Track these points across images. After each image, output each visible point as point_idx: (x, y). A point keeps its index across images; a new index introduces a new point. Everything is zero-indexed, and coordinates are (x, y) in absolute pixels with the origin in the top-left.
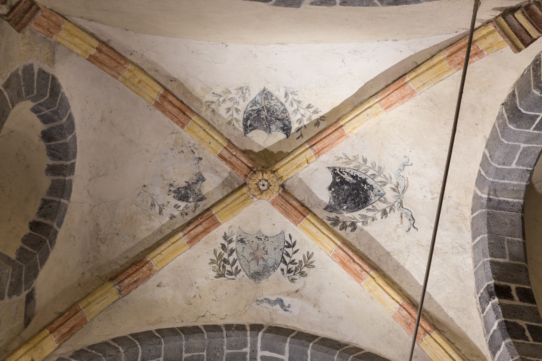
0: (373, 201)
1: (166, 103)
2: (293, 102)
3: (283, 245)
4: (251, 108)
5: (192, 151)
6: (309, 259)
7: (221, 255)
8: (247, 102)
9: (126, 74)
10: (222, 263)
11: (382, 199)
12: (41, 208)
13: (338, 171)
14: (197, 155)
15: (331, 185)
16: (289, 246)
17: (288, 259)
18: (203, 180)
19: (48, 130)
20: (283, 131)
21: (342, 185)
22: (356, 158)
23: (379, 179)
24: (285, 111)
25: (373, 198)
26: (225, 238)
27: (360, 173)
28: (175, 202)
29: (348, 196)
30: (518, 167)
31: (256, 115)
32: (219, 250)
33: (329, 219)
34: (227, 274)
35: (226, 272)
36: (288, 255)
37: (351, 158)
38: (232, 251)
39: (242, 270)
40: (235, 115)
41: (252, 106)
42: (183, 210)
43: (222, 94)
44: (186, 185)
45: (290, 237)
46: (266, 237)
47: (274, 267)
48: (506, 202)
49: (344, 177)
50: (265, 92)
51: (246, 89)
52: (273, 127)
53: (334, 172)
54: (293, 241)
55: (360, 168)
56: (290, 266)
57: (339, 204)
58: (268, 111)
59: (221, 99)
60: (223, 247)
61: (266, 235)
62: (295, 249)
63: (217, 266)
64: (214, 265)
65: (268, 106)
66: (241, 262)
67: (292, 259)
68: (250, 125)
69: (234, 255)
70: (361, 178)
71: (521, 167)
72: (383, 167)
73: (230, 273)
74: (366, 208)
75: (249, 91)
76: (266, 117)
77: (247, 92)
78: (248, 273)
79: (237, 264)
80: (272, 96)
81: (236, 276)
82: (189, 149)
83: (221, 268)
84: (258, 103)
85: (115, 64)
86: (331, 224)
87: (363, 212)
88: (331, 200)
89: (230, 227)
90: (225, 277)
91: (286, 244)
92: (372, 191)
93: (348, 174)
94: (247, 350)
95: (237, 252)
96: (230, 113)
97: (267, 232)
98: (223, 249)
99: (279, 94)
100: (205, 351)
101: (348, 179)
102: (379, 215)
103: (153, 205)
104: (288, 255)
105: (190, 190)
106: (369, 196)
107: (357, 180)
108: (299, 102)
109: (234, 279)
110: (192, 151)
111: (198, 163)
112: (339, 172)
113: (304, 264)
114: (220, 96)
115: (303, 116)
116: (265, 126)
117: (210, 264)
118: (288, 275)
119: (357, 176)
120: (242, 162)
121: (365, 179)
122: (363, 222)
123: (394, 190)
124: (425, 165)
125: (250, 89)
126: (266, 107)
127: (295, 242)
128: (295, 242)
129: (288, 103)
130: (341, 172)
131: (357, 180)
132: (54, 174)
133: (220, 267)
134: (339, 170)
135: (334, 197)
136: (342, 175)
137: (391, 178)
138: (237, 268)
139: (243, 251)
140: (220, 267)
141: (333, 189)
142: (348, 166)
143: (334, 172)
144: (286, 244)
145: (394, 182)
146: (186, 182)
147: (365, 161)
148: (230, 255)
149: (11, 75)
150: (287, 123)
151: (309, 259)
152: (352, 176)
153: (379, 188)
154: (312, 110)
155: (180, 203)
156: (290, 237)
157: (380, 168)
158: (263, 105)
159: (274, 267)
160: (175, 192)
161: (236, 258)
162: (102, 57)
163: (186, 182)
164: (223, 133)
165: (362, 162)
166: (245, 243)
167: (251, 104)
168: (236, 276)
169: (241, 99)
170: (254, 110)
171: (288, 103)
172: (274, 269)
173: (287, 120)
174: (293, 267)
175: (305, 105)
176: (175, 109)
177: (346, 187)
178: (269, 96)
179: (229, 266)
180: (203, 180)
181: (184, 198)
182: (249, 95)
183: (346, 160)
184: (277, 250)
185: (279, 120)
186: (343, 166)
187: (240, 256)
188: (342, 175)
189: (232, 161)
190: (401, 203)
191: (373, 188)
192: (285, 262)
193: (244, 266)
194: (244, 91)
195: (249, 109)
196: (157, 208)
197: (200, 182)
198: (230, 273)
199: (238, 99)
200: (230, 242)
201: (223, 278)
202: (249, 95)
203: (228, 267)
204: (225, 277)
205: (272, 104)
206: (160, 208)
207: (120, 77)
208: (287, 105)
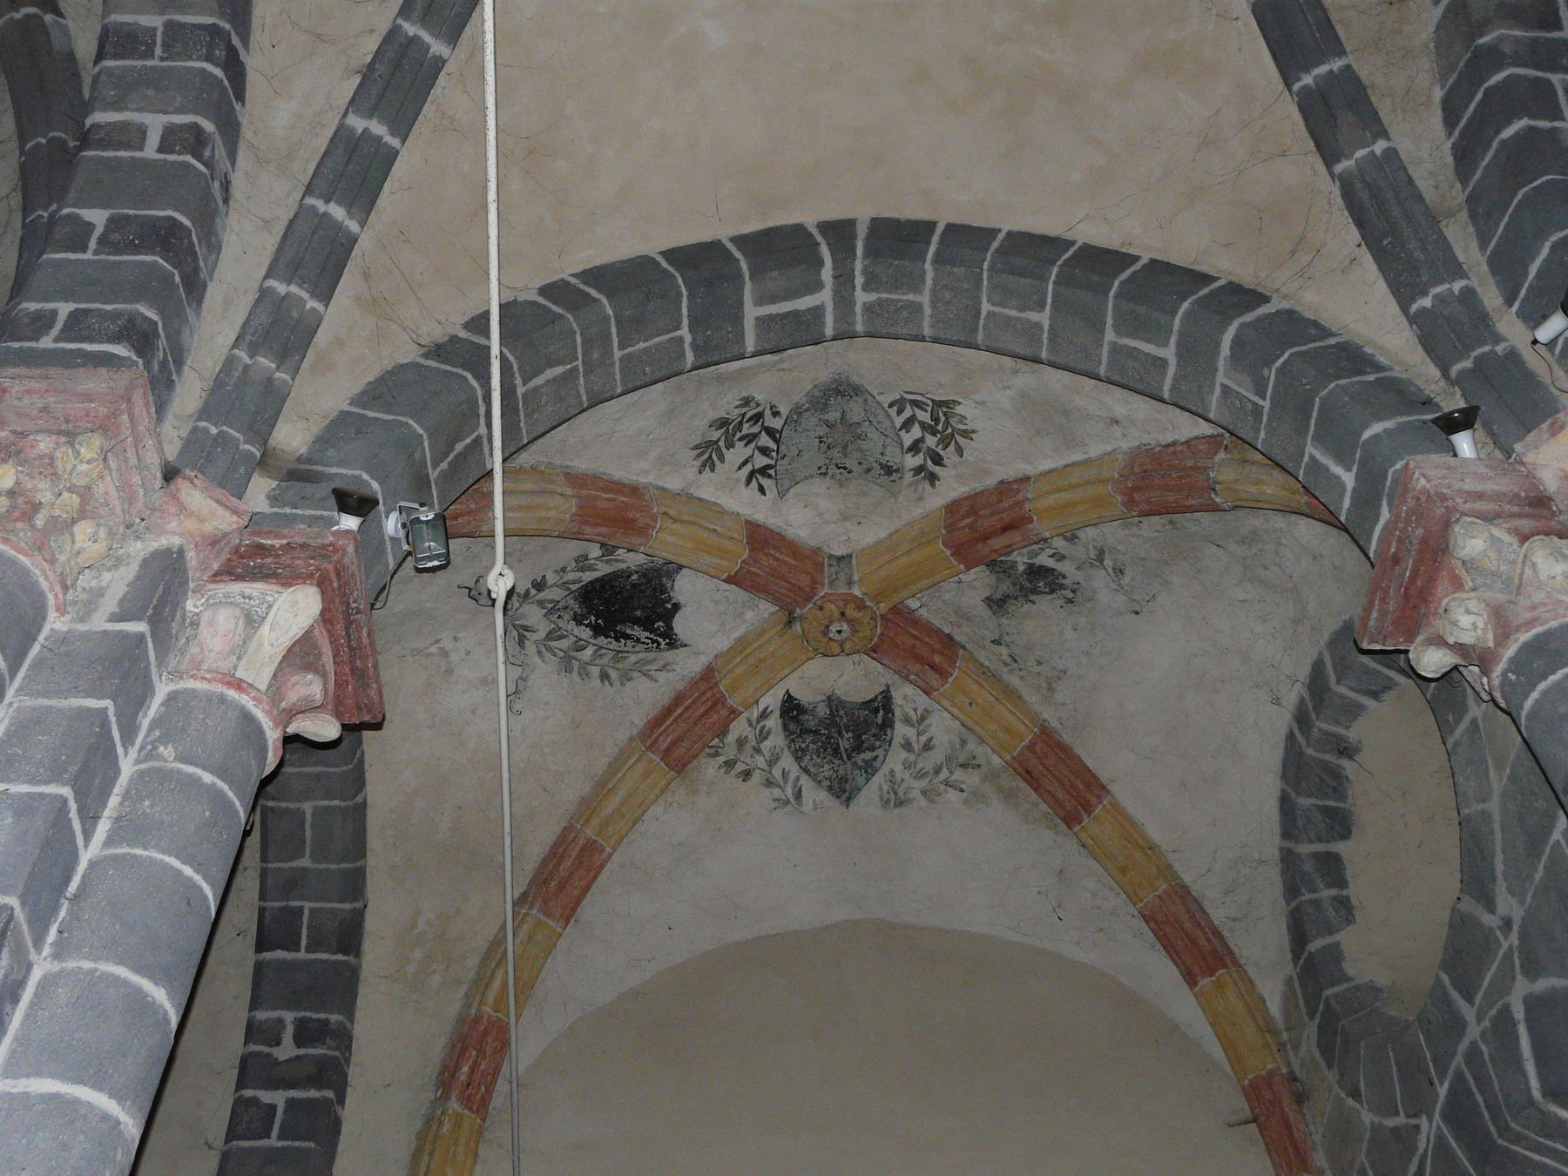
8: (885, 770)
14: (1003, 650)
16: (763, 471)
17: (765, 440)
18: (989, 601)
19: (1334, 839)
22: (626, 678)
23: (564, 644)
26: (933, 478)
28: (1064, 567)
30: (298, 805)
32: (949, 455)
36: (764, 451)
37: (635, 674)
38: (915, 448)
40: (910, 732)
41: (875, 759)
43: (942, 787)
45: (762, 490)
51: (888, 801)
52: (823, 711)
54: (754, 484)
58: (836, 751)
59: (944, 774)
60: (938, 460)
66: (887, 423)
67: (752, 445)
68: (876, 711)
69: (908, 439)
71: (290, 805)
73: (915, 403)
76: (840, 733)
77: (885, 796)
79: (899, 421)
80: (830, 789)
84: (860, 768)
87: (588, 577)
89: (920, 499)
91: (772, 472)
94: (862, 297)
96: (923, 739)
97: (819, 486)
99: (814, 794)
100: (984, 314)
101: (637, 632)
102: (551, 578)
104: (764, 451)
107: (616, 632)
108: (769, 783)
113: (721, 443)
114: (946, 783)
115: (758, 750)
118: (760, 409)
119: (617, 640)
121: (596, 635)
123: (526, 629)
124: (473, 712)
129: (793, 776)
131: (616, 632)
135: (664, 591)
137: (539, 652)
138: (900, 412)
139: (885, 447)
142: (641, 655)
144: (772, 472)
145: (531, 648)
147: (604, 676)
148: (922, 440)
150: (792, 726)
152: (627, 637)
153: (561, 623)
154: (740, 767)
155: (1051, 563)
156: (762, 490)
157: (568, 670)
158: (849, 765)
160: (1062, 587)
161: (902, 433)
169: (899, 776)
171: (793, 776)
172: (798, 411)
173: (792, 733)
175: (757, 777)
177: (638, 613)
180: (989, 601)
181: (1035, 572)
182: (881, 788)
185: (811, 731)
186: (651, 655)
189: (918, 666)
192: (770, 432)
194: (892, 797)
195: (880, 752)
196: (1108, 562)
197: (998, 596)
198: (915, 403)
199: (907, 776)
200: (919, 469)
202: (881, 788)
203: (924, 416)
205: (827, 767)
206: (1101, 561)
208: (794, 770)
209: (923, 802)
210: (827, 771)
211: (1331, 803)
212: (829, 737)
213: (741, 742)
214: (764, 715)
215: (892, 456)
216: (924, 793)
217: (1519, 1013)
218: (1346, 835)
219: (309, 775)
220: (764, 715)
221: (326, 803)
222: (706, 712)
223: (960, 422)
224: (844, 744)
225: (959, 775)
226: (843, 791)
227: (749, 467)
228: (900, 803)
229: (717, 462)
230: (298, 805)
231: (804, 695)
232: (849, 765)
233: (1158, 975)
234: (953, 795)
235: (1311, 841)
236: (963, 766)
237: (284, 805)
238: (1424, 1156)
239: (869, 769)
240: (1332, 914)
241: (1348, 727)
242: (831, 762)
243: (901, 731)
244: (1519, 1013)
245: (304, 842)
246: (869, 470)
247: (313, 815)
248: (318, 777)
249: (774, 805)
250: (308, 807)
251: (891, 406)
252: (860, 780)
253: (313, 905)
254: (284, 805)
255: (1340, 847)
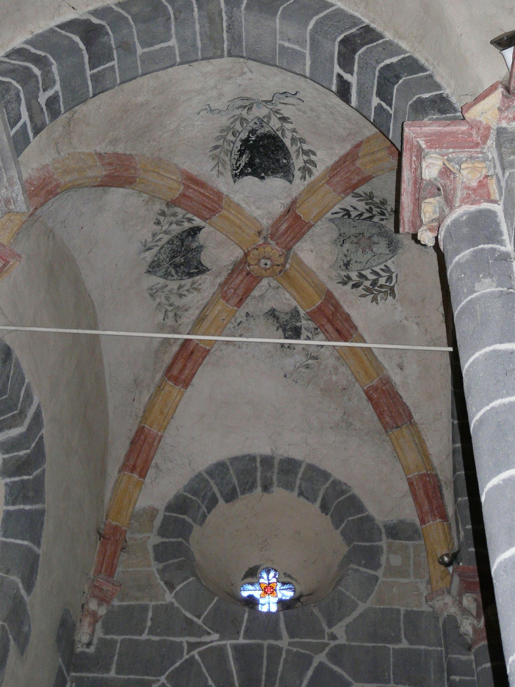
0: (270, 129)
1: (183, 377)
2: (155, 240)
3: (348, 220)
4: (175, 275)
5: (239, 324)
6: (362, 196)
7: (367, 289)
8: (168, 282)
9: (154, 430)
10: (376, 288)
11: (265, 120)
12: (308, 499)
13: (237, 172)
14: (244, 319)
15: (258, 177)
16: (349, 216)
19: (224, 498)
20: (197, 234)
21: (254, 165)
24: (170, 242)
25: (266, 130)
26: (345, 283)
27: (235, 148)
29: (269, 158)
31: (182, 267)
32: (360, 290)
33: (304, 178)
34: (390, 283)
35: (388, 284)
38: (361, 276)
39: (385, 264)
41: (172, 276)
42: (311, 333)
43: (164, 310)
44: (280, 330)
46: (340, 235)
47: (379, 227)
48: (229, 29)
49: (243, 164)
50: (151, 270)
51: (152, 289)
52: (194, 245)
53: (239, 175)
54: (340, 211)
55: (227, 150)
56: (374, 212)
57: (281, 168)
58: (174, 257)
60: (356, 286)
61: (337, 236)
62: (351, 209)
63: (380, 294)
64: (379, 298)
65: (168, 259)
66: (374, 264)
68: (197, 268)
69: (365, 273)
70: (241, 146)
71: (173, 31)
72: (219, 129)
73: (389, 279)
74: (281, 138)
75: (153, 286)
76: (183, 256)
78: (389, 256)
79: (377, 269)
80: (154, 261)
81: (393, 273)
82: (236, 328)
83: (383, 290)
84: (166, 271)
85: (146, 446)
86: (310, 176)
87: (287, 142)
88: (278, 176)
90: (394, 286)
92: (257, 130)
93: (238, 160)
95: (362, 270)
96: (185, 293)
98: (359, 286)
99: (149, 256)
101: (245, 159)
103: (307, 367)
105: (287, 325)
106: (265, 135)
107: (244, 150)
108: (154, 235)
109: (397, 275)
110: (239, 324)
111: (252, 316)
112: (239, 171)
113: (370, 201)
115: (171, 224)
116: (194, 253)
117: (377, 303)
120: (242, 281)
121: (242, 141)
122: (301, 142)
125: (150, 286)
126: (170, 261)
127: (340, 209)
128: (340, 209)
130: (238, 168)
131: (244, 150)
132: (271, 484)
133: (381, 292)
134: (235, 170)
136: (241, 167)
137: (234, 116)
140: (381, 292)
141: (263, 175)
142: (228, 162)
143: (239, 175)
146: (277, 329)
147: (216, 147)
148: (367, 279)
149: (162, 580)
150: (185, 234)
151: (362, 196)
152: (241, 155)
154: (162, 218)
159: (379, 227)
161: (370, 271)
162: (140, 463)
163: (277, 329)
164: (212, 293)
165: (218, 150)
166: (350, 261)
167: (170, 278)
168: (393, 273)
170: (176, 271)
173: (181, 235)
174: (375, 211)
176: (188, 366)
177: (257, 160)
178: (155, 264)
179: (380, 279)
182: (158, 284)
183: (220, 166)
184: (355, 224)
186: (229, 167)
187: (367, 266)
188: (241, 167)
190: (266, 102)
191: (253, 130)
192: (371, 218)
193: (381, 261)
194: (155, 291)
195: (176, 277)
196: (310, 362)
198: (389, 279)
200: (349, 278)
201: (395, 288)
202: (158, 284)
203: (382, 281)
204: (394, 286)
205: (164, 256)
206: (310, 359)
207: (160, 433)
209: (155, 305)
210: (163, 257)
211: (238, 489)
212: (180, 252)
213: (175, 215)
214: (190, 220)
215: (354, 266)
216: (159, 304)
217: (315, 664)
218: (227, 501)
219: (195, 39)
220: (190, 220)
221: (177, 53)
222: (207, 208)
223: (382, 298)
224: (177, 260)
225: (171, 314)
226: (153, 268)
227: (351, 209)
228: (152, 295)
229: (358, 199)
230: (174, 36)
231: (201, 236)
232: (167, 265)
233: (119, 450)
234: (161, 317)
235: (219, 490)
236: (176, 315)
237: (173, 27)
238: (205, 643)
239: (167, 275)
240: (199, 516)
241: (278, 486)
242: (167, 257)
243: (187, 282)
244: (315, 664)
245: (151, 45)
246: (345, 256)
247: (169, 47)
248: (194, 45)
249: (143, 241)
250: (173, 42)
251: (385, 266)
252: (160, 273)
253: (116, 66)
254: (173, 27)
255: (221, 501)
